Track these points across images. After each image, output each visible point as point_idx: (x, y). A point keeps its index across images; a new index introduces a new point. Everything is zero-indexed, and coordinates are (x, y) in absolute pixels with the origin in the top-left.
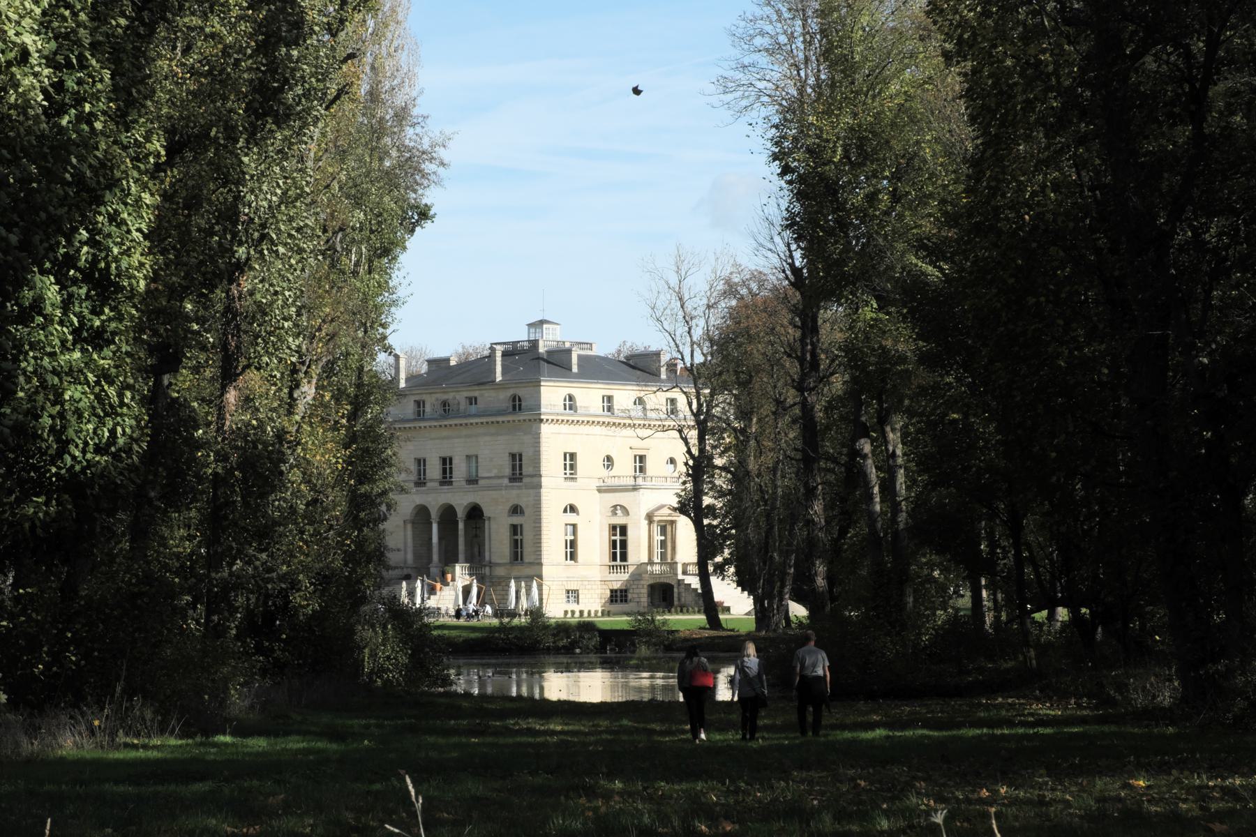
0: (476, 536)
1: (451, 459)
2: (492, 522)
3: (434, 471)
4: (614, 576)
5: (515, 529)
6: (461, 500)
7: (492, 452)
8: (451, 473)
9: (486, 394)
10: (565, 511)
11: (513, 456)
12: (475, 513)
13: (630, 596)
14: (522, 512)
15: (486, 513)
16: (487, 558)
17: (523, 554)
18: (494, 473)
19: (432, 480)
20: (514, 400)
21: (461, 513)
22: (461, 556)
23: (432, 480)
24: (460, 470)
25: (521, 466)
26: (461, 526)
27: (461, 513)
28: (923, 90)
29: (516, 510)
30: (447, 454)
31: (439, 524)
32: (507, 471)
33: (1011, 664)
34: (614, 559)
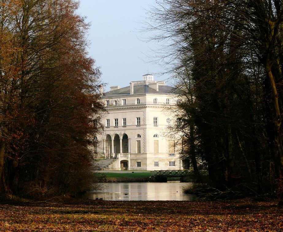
0: (126, 145)
4: (170, 157)
5: (139, 142)
6: (121, 133)
7: (131, 117)
9: (129, 98)
10: (154, 136)
12: (125, 137)
13: (176, 164)
14: (140, 137)
15: (129, 137)
17: (146, 164)
18: (131, 124)
22: (121, 151)
24: (121, 123)
25: (140, 121)
26: (121, 141)
28: (221, 24)
30: (116, 118)
33: (278, 62)
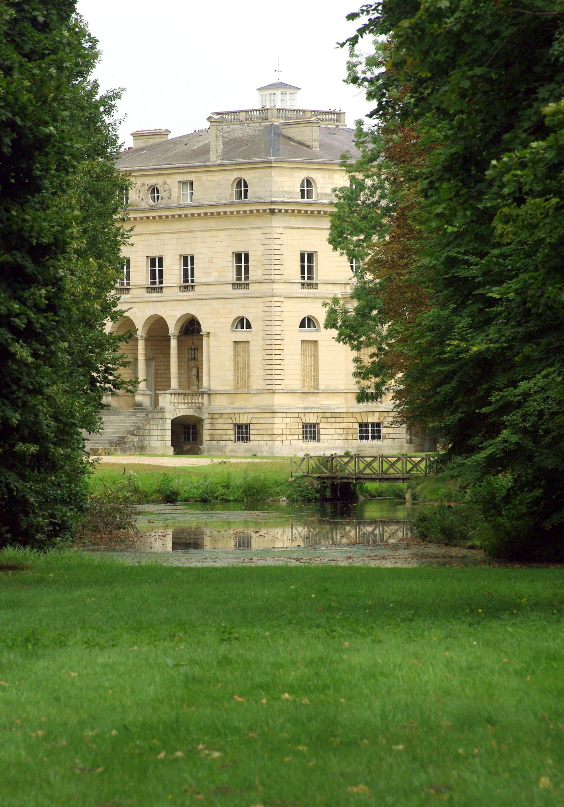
0: (194, 359)
1: (161, 260)
2: (211, 338)
3: (173, 273)
8: (161, 276)
10: (302, 325)
11: (153, 261)
12: (191, 328)
14: (249, 326)
15: (204, 329)
16: (205, 383)
19: (137, 287)
20: (239, 184)
21: (173, 329)
23: (137, 287)
24: (173, 273)
26: (174, 343)
27: (173, 329)
29: (243, 323)
30: (155, 253)
31: (146, 340)
32: (231, 276)
34: (303, 278)
